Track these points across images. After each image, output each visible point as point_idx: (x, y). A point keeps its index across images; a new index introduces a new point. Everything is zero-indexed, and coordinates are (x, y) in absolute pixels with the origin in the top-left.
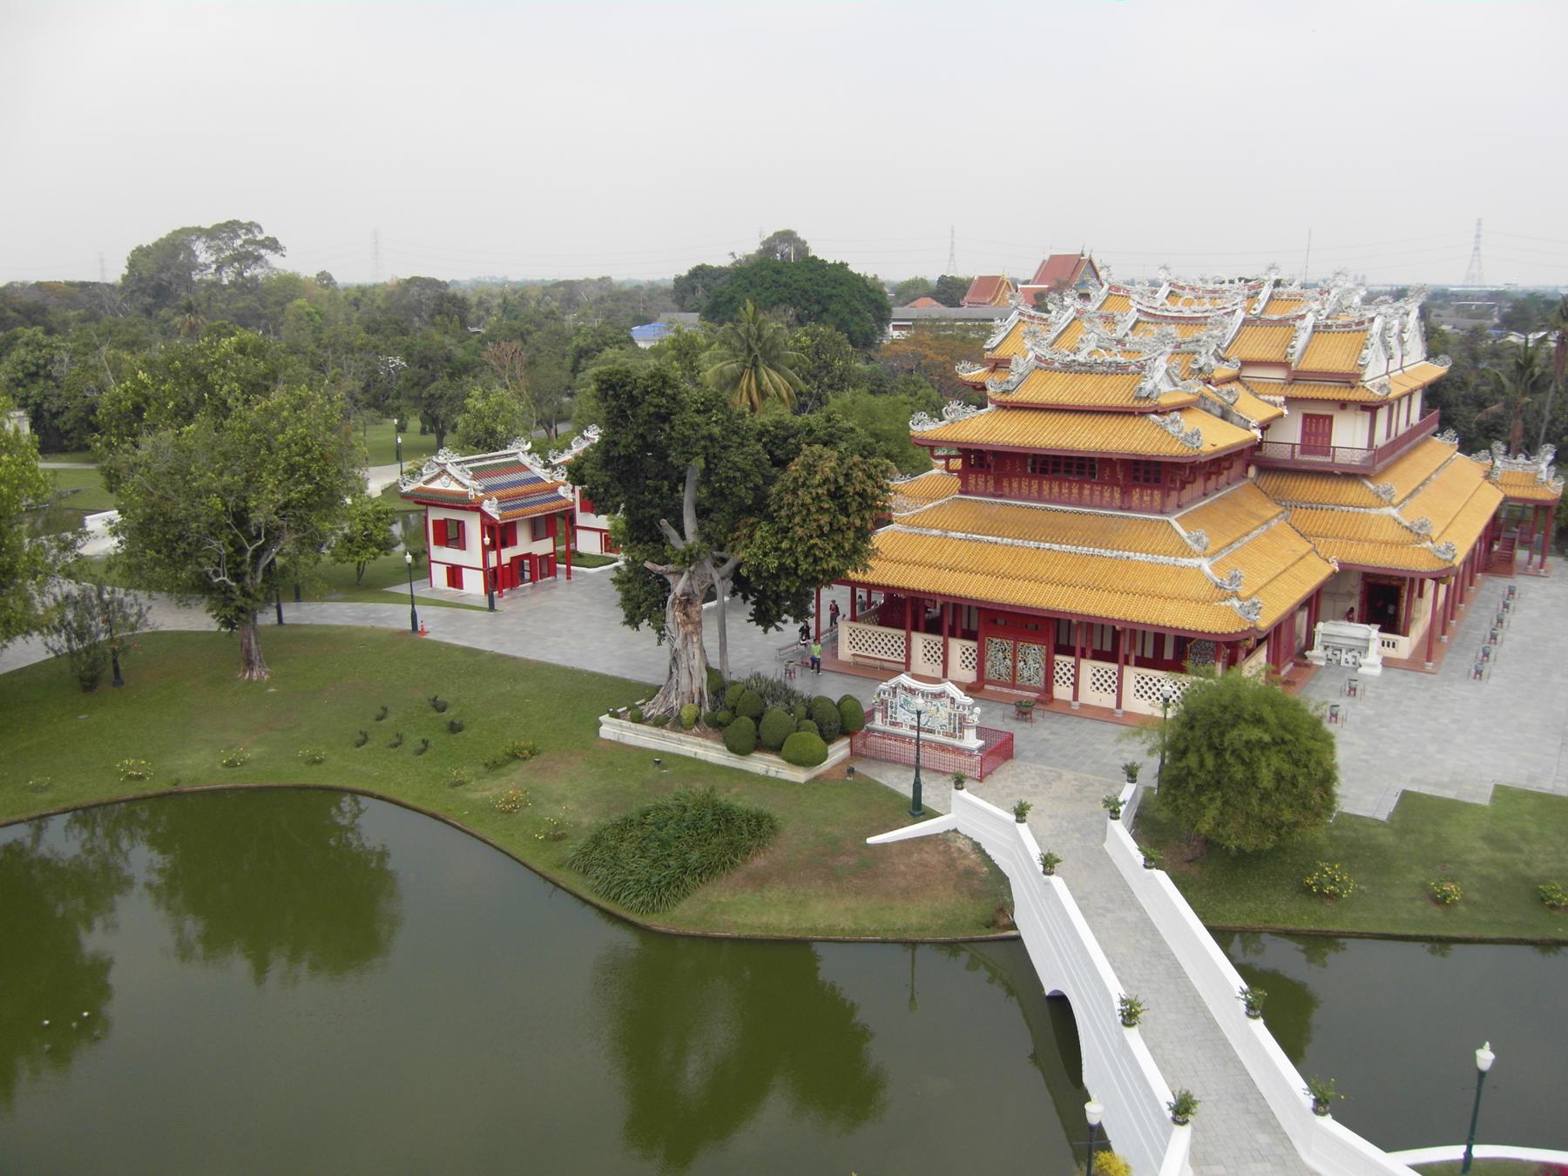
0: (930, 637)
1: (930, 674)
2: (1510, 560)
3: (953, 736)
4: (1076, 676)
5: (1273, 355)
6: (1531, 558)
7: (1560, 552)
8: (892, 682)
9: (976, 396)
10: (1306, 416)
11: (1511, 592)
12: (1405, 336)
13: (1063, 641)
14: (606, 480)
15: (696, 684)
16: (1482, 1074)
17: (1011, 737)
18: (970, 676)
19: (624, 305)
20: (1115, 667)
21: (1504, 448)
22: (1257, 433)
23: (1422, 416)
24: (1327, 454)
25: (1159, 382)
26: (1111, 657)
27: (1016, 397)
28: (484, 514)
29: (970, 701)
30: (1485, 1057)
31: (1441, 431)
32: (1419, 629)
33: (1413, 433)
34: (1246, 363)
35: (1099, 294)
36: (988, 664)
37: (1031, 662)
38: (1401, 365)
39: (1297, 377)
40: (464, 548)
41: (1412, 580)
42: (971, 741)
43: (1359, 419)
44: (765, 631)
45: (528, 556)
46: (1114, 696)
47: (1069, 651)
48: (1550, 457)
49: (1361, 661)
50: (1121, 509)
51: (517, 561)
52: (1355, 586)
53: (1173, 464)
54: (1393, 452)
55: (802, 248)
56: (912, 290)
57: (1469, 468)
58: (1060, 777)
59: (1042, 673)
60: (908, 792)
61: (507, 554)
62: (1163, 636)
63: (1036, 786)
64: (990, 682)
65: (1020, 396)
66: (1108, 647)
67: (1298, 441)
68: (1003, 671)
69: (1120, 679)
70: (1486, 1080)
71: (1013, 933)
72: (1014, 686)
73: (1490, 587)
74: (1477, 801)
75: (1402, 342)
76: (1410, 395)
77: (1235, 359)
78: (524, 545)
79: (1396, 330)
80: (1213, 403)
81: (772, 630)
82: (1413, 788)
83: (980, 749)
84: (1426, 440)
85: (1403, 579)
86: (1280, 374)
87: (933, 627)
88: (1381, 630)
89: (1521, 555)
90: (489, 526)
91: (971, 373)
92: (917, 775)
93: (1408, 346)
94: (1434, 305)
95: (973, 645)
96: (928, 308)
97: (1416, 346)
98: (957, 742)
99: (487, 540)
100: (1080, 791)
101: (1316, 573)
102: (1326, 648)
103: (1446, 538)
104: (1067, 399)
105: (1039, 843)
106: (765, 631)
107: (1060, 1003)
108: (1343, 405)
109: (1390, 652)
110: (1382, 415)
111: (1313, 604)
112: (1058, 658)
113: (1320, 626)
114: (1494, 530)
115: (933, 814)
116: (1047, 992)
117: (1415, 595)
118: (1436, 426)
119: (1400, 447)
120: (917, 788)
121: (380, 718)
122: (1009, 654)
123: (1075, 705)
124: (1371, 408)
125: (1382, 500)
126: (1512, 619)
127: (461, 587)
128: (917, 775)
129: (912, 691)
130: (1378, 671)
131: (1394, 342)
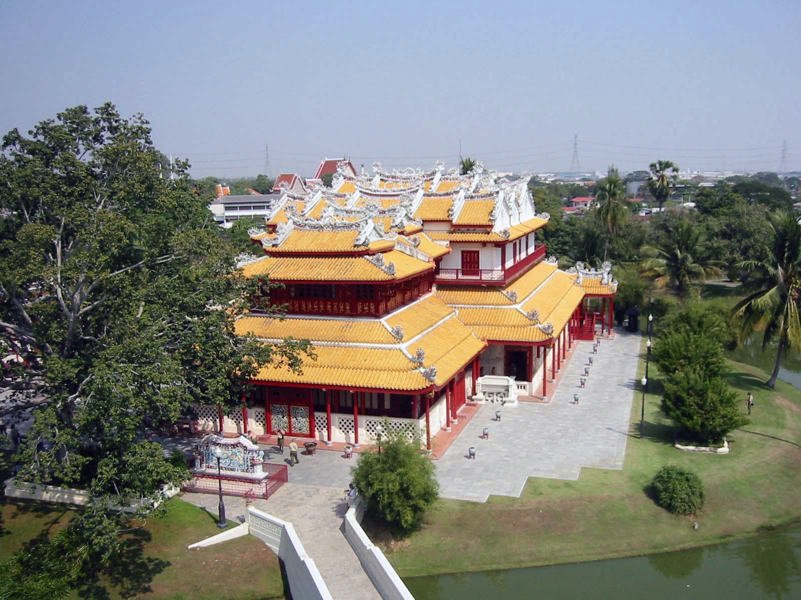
5: (443, 216)
9: (256, 248)
10: (463, 252)
20: (352, 417)
25: (369, 235)
27: (279, 249)
33: (529, 258)
38: (518, 217)
39: (458, 228)
42: (259, 473)
43: (494, 252)
47: (322, 409)
52: (500, 353)
53: (380, 286)
54: (516, 271)
62: (383, 395)
63: (302, 499)
67: (460, 267)
75: (518, 205)
76: (527, 235)
77: (419, 219)
79: (513, 199)
82: (534, 475)
84: (539, 262)
89: (598, 327)
92: (221, 498)
93: (522, 208)
101: (474, 347)
102: (484, 393)
103: (548, 321)
107: (203, 509)
108: (484, 244)
110: (509, 248)
112: (317, 414)
115: (233, 525)
120: (222, 510)
124: (500, 245)
125: (513, 299)
128: (221, 498)
130: (516, 404)
131: (512, 205)
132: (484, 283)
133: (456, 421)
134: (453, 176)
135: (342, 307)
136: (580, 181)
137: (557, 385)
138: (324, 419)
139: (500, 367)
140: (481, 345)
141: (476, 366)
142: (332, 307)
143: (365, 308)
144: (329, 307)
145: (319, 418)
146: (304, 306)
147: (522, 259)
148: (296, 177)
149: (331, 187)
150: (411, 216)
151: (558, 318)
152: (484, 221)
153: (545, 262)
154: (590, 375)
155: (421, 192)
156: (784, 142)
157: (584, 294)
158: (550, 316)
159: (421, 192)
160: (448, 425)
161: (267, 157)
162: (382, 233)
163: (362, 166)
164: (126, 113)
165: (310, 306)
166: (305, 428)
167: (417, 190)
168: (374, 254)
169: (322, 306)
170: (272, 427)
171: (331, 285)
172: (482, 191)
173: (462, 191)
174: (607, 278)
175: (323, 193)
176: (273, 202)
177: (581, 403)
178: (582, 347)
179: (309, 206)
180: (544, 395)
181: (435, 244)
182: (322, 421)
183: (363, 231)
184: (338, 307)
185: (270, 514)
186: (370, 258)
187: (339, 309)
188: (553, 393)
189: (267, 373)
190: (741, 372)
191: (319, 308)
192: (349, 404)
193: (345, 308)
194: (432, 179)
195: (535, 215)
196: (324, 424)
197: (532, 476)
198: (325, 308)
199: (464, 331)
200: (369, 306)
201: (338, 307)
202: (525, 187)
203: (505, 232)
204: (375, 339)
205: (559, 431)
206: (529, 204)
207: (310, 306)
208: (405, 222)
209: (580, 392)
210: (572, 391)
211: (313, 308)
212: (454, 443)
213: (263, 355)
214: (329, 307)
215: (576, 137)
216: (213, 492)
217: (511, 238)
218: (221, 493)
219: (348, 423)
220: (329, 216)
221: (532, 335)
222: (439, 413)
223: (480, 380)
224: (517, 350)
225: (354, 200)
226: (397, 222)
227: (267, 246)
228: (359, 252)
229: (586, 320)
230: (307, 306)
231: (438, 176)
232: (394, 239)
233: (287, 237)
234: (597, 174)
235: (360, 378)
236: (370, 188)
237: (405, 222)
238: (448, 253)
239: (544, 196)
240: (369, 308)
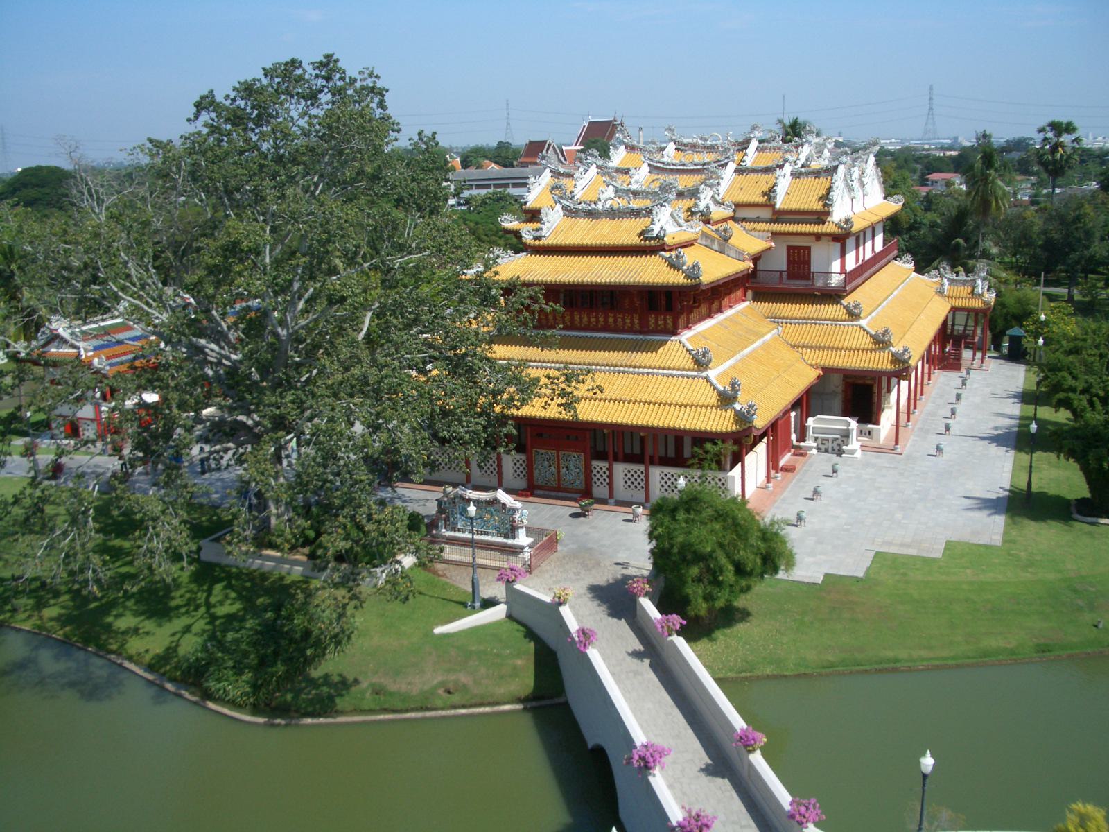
2: (958, 357)
3: (506, 536)
4: (610, 477)
6: (974, 355)
9: (516, 244)
10: (789, 248)
13: (600, 448)
16: (925, 776)
20: (642, 468)
27: (544, 242)
30: (928, 762)
32: (888, 417)
33: (877, 258)
34: (738, 205)
36: (536, 472)
37: (572, 467)
38: (863, 200)
39: (780, 216)
46: (643, 491)
47: (602, 456)
49: (844, 447)
50: (641, 332)
57: (927, 282)
59: (582, 477)
65: (549, 240)
67: (785, 269)
69: (647, 477)
70: (928, 781)
71: (561, 700)
74: (933, 556)
75: (863, 185)
83: (530, 546)
85: (873, 379)
86: (766, 213)
89: (967, 354)
91: (509, 222)
93: (868, 188)
95: (522, 457)
98: (510, 542)
101: (805, 377)
102: (816, 439)
104: (589, 240)
105: (578, 620)
108: (818, 236)
110: (851, 242)
112: (595, 463)
117: (884, 391)
118: (896, 252)
119: (866, 270)
122: (554, 463)
131: (856, 184)
132: (817, 290)
133: (779, 475)
134: (775, 144)
135: (628, 321)
136: (936, 149)
137: (913, 430)
138: (604, 469)
139: (837, 403)
140: (812, 375)
141: (807, 403)
142: (615, 321)
143: (660, 323)
144: (611, 320)
145: (598, 469)
147: (867, 258)
148: (550, 145)
149: (609, 158)
150: (718, 198)
151: (916, 339)
152: (818, 206)
153: (897, 263)
154: (958, 418)
155: (732, 166)
157: (949, 307)
158: (907, 336)
159: (732, 166)
160: (768, 481)
161: (508, 118)
162: (681, 221)
163: (641, 129)
164: (351, 66)
165: (585, 319)
166: (578, 482)
167: (727, 164)
168: (670, 250)
169: (601, 319)
170: (535, 479)
172: (814, 165)
173: (787, 165)
174: (980, 285)
175: (599, 167)
176: (532, 179)
177: (945, 456)
178: (943, 380)
179: (580, 184)
180: (897, 443)
181: (750, 241)
182: (601, 472)
183: (656, 219)
185: (538, 591)
186: (667, 255)
187: (624, 323)
188: (908, 440)
189: (533, 410)
191: (597, 321)
192: (637, 450)
193: (632, 323)
194: (746, 148)
195: (885, 198)
196: (605, 476)
197: (881, 550)
198: (606, 320)
199: (789, 355)
200: (665, 320)
202: (872, 160)
203: (847, 221)
204: (673, 364)
206: (876, 182)
207: (585, 319)
208: (712, 207)
209: (944, 441)
210: (934, 440)
211: (589, 322)
212: (776, 505)
213: (528, 389)
214: (611, 320)
216: (466, 565)
217: (854, 230)
218: (473, 566)
219: (636, 476)
220: (607, 197)
221: (880, 362)
222: (757, 459)
223: (811, 422)
224: (860, 382)
225: (642, 177)
226: (702, 206)
227: (527, 238)
228: (650, 247)
229: (949, 346)
230: (581, 319)
231: (754, 145)
232: (697, 230)
233: (555, 226)
234: (960, 140)
235: (653, 415)
236: (663, 160)
237: (712, 207)
239: (900, 168)
240: (665, 323)
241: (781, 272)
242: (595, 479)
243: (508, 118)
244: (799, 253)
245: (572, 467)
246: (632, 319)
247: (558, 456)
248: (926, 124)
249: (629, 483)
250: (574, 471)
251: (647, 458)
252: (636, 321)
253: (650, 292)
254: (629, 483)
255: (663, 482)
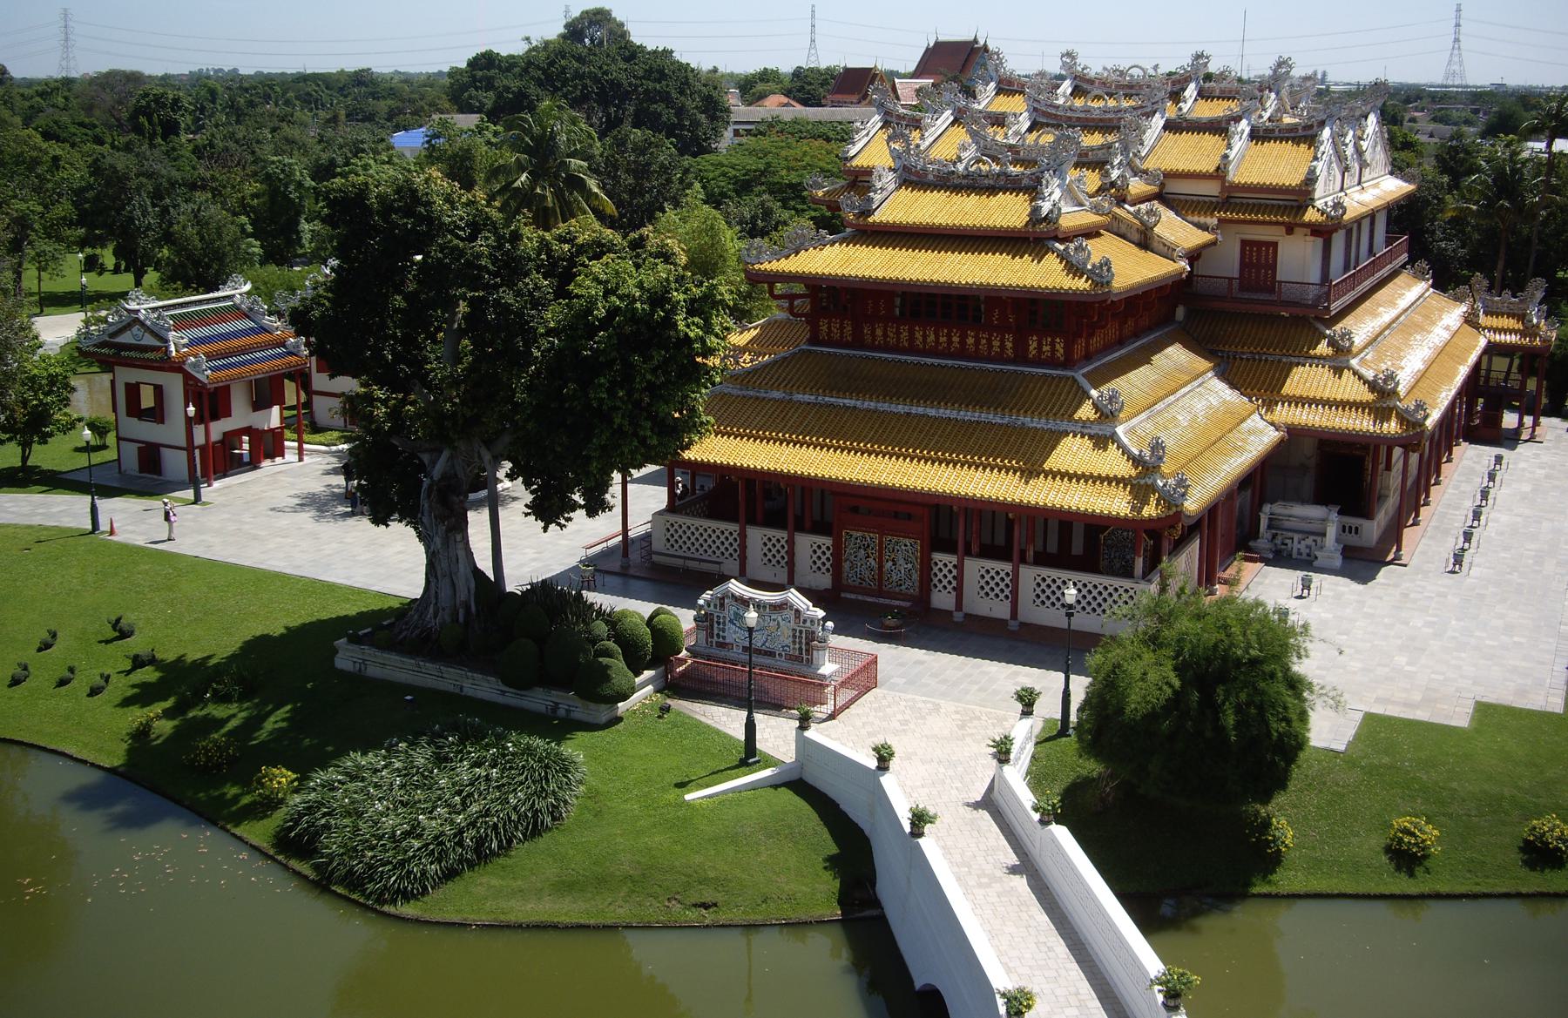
0: (771, 532)
1: (777, 581)
6: (1521, 420)
7: (1555, 411)
8: (719, 590)
10: (1244, 243)
11: (1499, 459)
12: (1364, 145)
14: (337, 332)
15: (462, 595)
17: (875, 661)
18: (824, 581)
19: (366, 100)
20: (1008, 567)
21: (1486, 283)
22: (1184, 264)
23: (1388, 242)
24: (1271, 290)
26: (1001, 554)
28: (188, 377)
29: (821, 613)
31: (1411, 261)
35: (185, 120)
36: (846, 565)
40: (162, 422)
41: (1377, 448)
44: (545, 529)
45: (248, 431)
46: (1008, 603)
47: (949, 548)
48: (1539, 295)
51: (231, 438)
55: (619, 34)
56: (753, 86)
58: (937, 708)
59: (915, 576)
60: (741, 735)
61: (218, 428)
63: (906, 722)
64: (852, 589)
66: (1000, 540)
67: (1236, 275)
68: (866, 574)
71: (874, 912)
72: (880, 593)
73: (1470, 459)
78: (240, 416)
80: (1130, 225)
81: (552, 526)
82: (1378, 709)
85: (1365, 447)
87: (773, 520)
88: (1340, 513)
90: (194, 390)
94: (1396, 106)
95: (827, 541)
96: (774, 106)
97: (1376, 154)
99: (191, 409)
100: (962, 727)
106: (545, 529)
109: (1352, 540)
110: (1338, 240)
111: (1262, 481)
112: (937, 556)
113: (1267, 508)
114: (1474, 385)
116: (918, 985)
117: (1382, 467)
118: (1404, 257)
119: (1366, 285)
120: (750, 727)
121: (45, 646)
123: (958, 617)
126: (1499, 493)
127: (160, 473)
129: (745, 603)
135: (996, 343)
142: (977, 342)
143: (1045, 348)
144: (970, 341)
145: (940, 565)
146: (919, 335)
156: (66, 15)
161: (813, 32)
169: (956, 339)
171: (976, 298)
184: (989, 341)
187: (990, 346)
190: (1182, 166)
191: (950, 342)
193: (1002, 346)
198: (963, 342)
200: (1053, 344)
201: (989, 341)
205: (1429, 624)
214: (970, 341)
215: (1459, 10)
230: (925, 337)
238: (1214, 243)
240: (1053, 350)
241: (1231, 279)
242: (935, 581)
243: (813, 32)
244: (1259, 252)
245: (902, 562)
246: (1002, 342)
247: (881, 543)
248: (1450, 62)
249: (987, 589)
250: (903, 566)
251: (1016, 556)
252: (1009, 345)
253: (928, 295)
254: (987, 589)
255: (1038, 591)
